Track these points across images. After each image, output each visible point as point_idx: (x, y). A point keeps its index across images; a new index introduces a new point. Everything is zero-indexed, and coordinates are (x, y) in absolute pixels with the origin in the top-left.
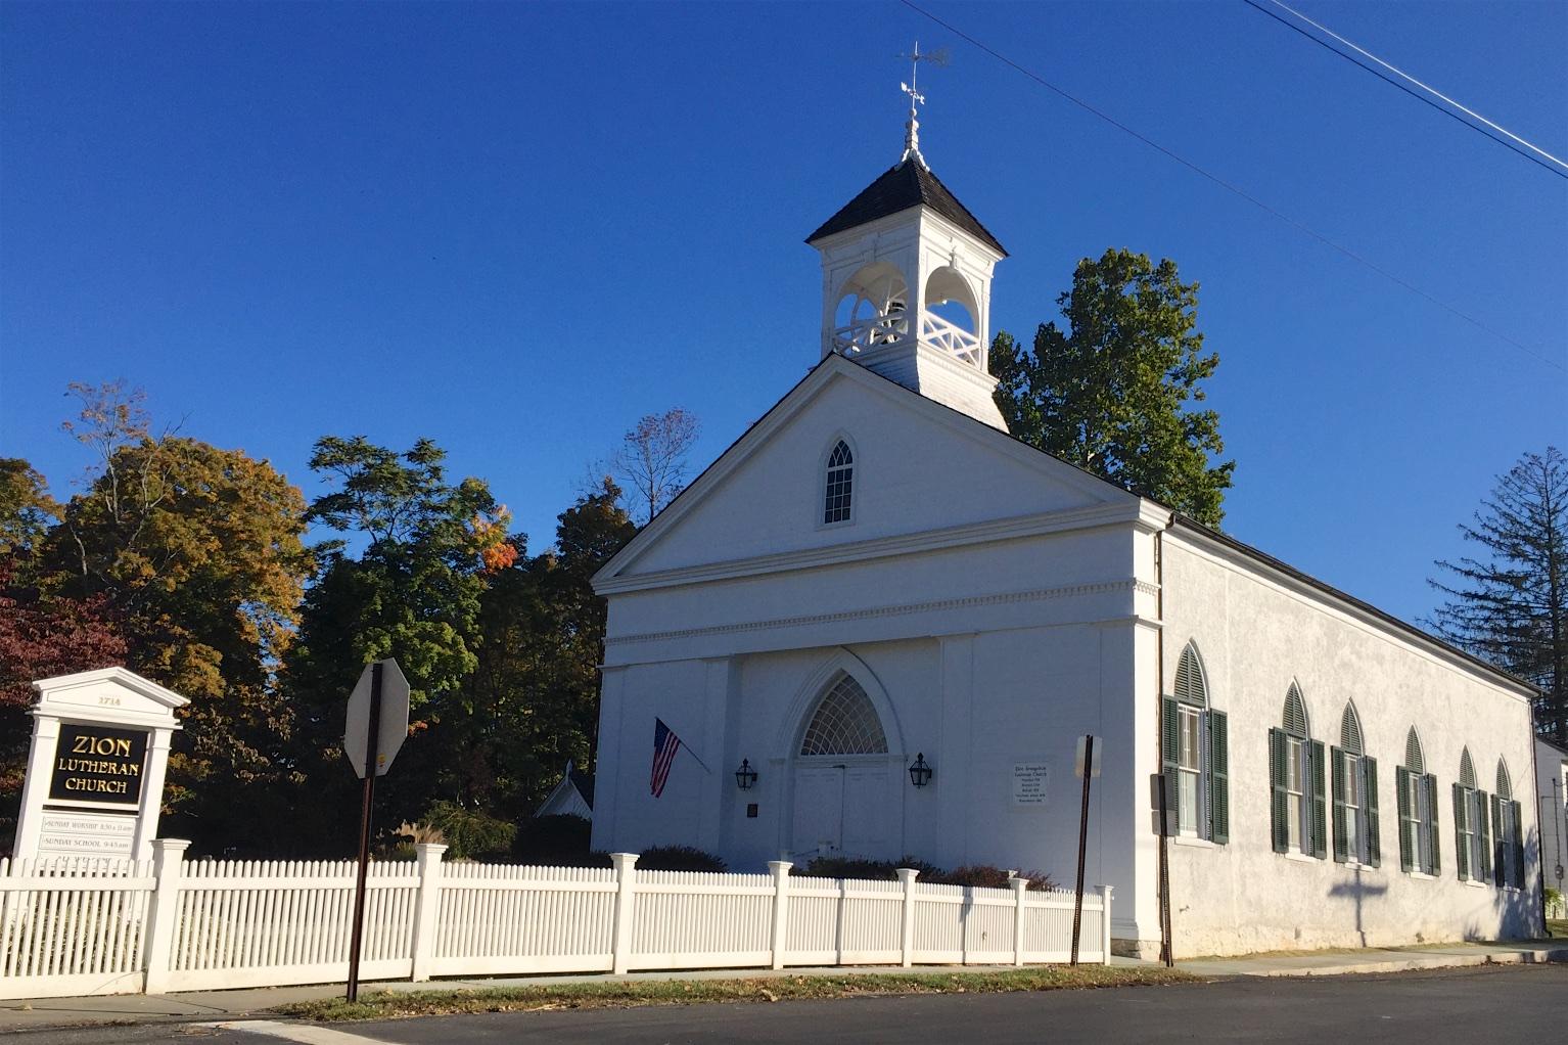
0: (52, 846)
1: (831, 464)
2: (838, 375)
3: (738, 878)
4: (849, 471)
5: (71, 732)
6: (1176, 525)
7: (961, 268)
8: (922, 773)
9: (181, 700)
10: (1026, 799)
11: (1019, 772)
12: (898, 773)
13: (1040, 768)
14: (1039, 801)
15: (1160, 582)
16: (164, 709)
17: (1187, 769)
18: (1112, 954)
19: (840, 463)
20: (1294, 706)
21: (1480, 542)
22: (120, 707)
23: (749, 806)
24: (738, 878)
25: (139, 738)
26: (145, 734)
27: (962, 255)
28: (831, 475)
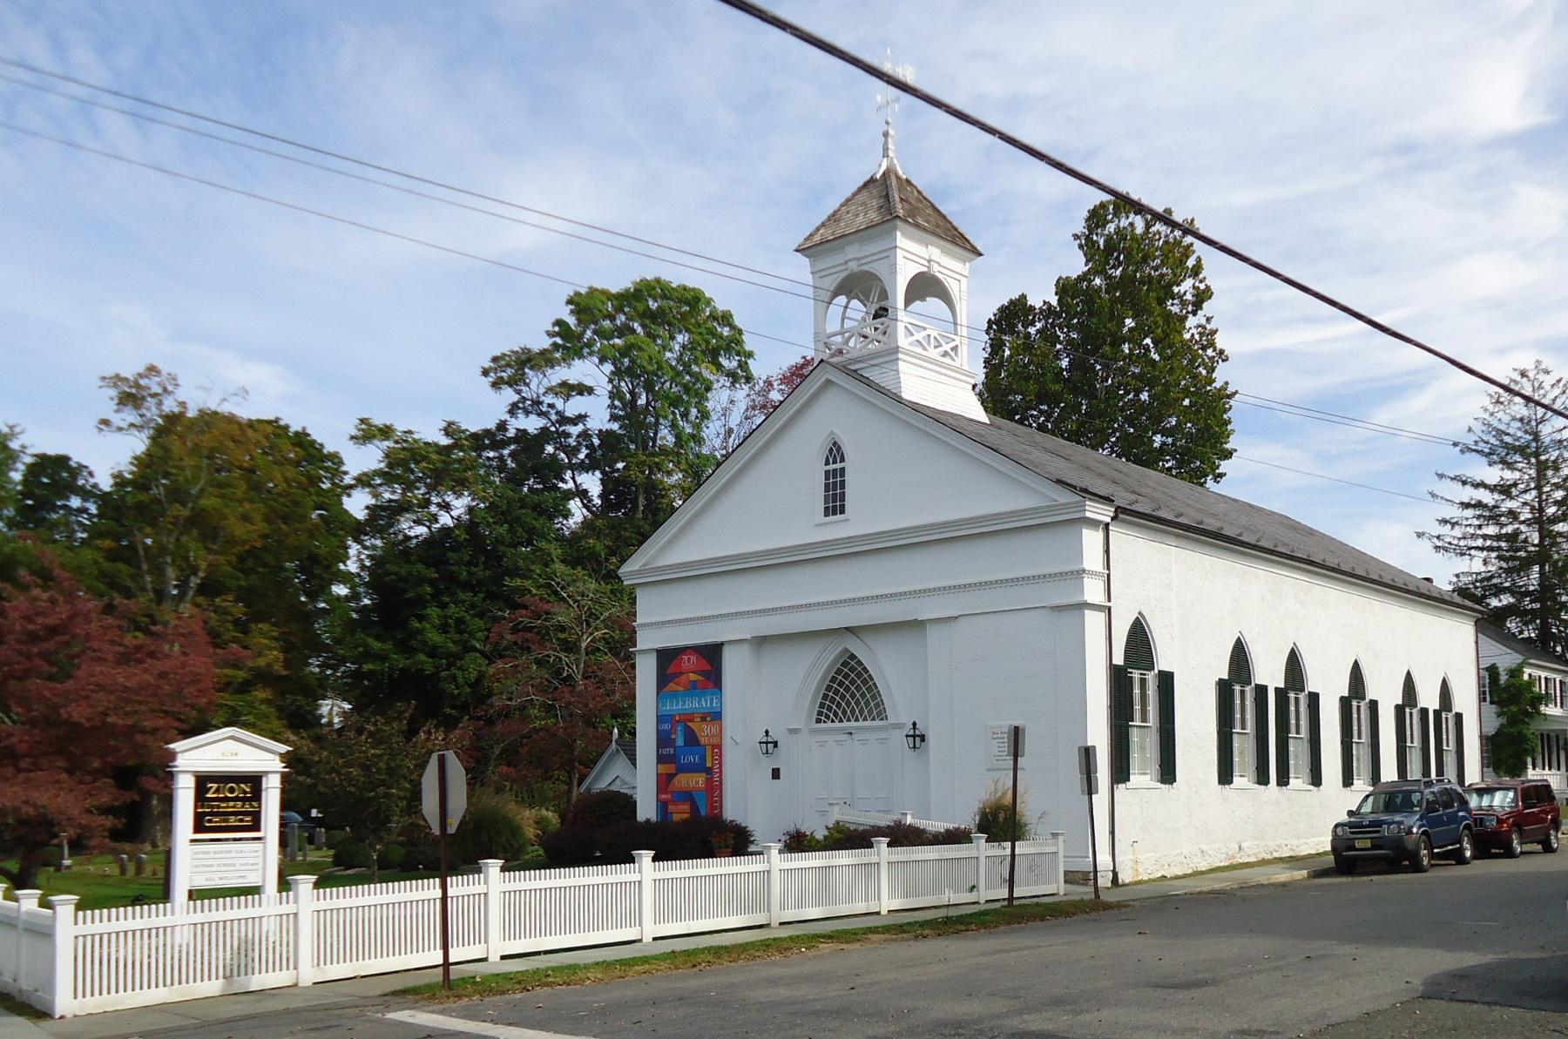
0: (198, 856)
1: (827, 463)
2: (829, 382)
4: (843, 469)
5: (202, 781)
6: (1121, 516)
7: (936, 270)
8: (917, 738)
9: (284, 748)
12: (899, 739)
15: (1108, 569)
16: (271, 756)
17: (1138, 724)
18: (1066, 882)
19: (835, 462)
20: (1240, 659)
21: (1474, 454)
23: (773, 769)
25: (254, 781)
26: (261, 777)
27: (938, 260)
28: (827, 473)
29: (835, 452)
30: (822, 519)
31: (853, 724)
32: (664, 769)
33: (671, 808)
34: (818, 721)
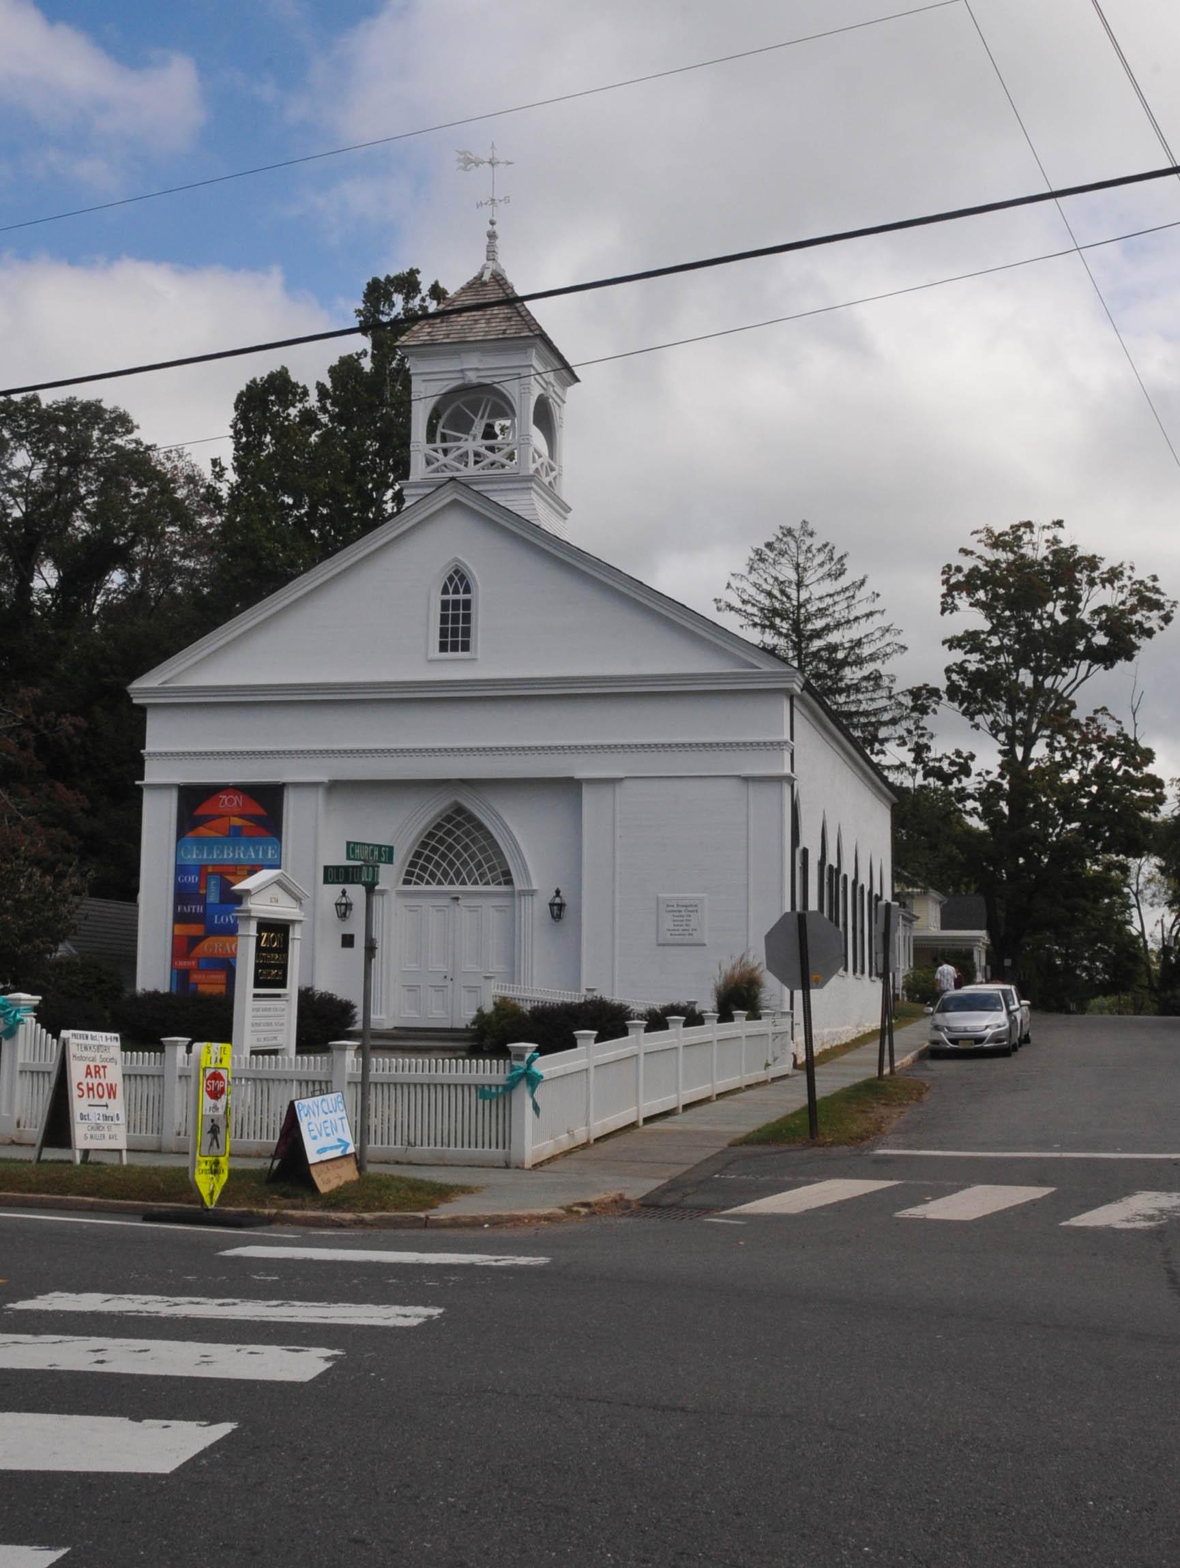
1: (445, 591)
2: (455, 503)
3: (264, 1060)
5: (944, 926)
10: (677, 933)
11: (670, 909)
13: (691, 906)
14: (690, 934)
19: (456, 591)
22: (193, 1074)
24: (264, 1060)
29: (458, 580)
30: (435, 653)
31: (457, 887)
32: (182, 929)
33: (195, 977)
34: (407, 882)
